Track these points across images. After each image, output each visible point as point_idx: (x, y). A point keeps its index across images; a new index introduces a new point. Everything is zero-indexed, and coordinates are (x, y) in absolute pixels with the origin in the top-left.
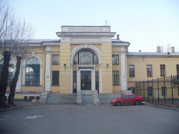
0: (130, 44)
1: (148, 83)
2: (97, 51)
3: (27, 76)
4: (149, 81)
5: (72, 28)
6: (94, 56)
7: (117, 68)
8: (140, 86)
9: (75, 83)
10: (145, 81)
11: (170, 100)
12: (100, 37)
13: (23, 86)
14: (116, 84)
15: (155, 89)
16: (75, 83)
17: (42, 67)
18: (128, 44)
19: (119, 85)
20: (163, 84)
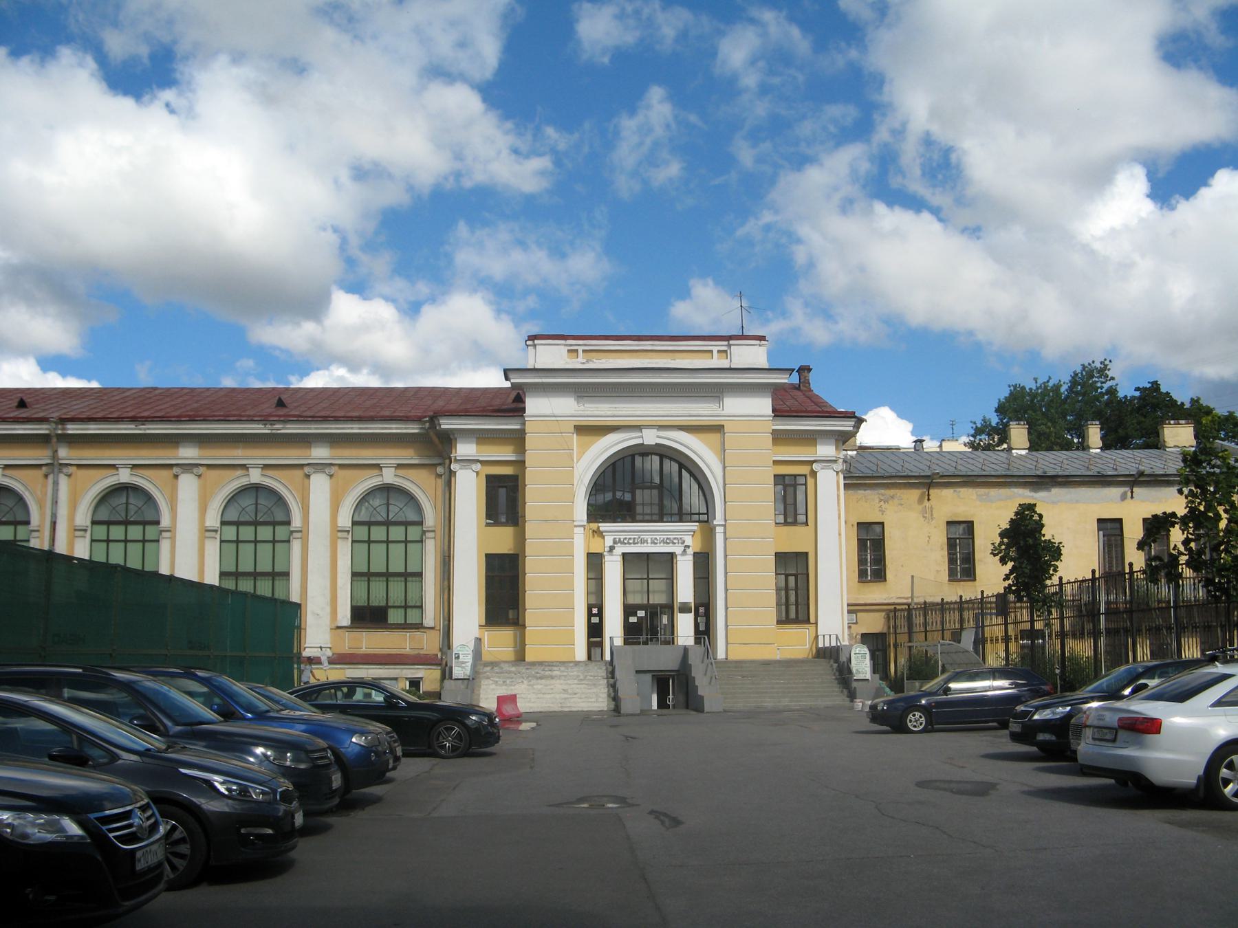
0: (864, 424)
1: (961, 610)
2: (150, 489)
3: (589, 581)
4: (967, 602)
5: (580, 349)
6: (685, 473)
7: (502, 540)
8: (926, 624)
9: (595, 620)
10: (929, 600)
11: (581, 664)
12: (716, 392)
13: (520, 657)
14: (793, 615)
15: (992, 640)
16: (702, 628)
17: (432, 535)
18: (852, 423)
19: (808, 621)
20: (1026, 618)
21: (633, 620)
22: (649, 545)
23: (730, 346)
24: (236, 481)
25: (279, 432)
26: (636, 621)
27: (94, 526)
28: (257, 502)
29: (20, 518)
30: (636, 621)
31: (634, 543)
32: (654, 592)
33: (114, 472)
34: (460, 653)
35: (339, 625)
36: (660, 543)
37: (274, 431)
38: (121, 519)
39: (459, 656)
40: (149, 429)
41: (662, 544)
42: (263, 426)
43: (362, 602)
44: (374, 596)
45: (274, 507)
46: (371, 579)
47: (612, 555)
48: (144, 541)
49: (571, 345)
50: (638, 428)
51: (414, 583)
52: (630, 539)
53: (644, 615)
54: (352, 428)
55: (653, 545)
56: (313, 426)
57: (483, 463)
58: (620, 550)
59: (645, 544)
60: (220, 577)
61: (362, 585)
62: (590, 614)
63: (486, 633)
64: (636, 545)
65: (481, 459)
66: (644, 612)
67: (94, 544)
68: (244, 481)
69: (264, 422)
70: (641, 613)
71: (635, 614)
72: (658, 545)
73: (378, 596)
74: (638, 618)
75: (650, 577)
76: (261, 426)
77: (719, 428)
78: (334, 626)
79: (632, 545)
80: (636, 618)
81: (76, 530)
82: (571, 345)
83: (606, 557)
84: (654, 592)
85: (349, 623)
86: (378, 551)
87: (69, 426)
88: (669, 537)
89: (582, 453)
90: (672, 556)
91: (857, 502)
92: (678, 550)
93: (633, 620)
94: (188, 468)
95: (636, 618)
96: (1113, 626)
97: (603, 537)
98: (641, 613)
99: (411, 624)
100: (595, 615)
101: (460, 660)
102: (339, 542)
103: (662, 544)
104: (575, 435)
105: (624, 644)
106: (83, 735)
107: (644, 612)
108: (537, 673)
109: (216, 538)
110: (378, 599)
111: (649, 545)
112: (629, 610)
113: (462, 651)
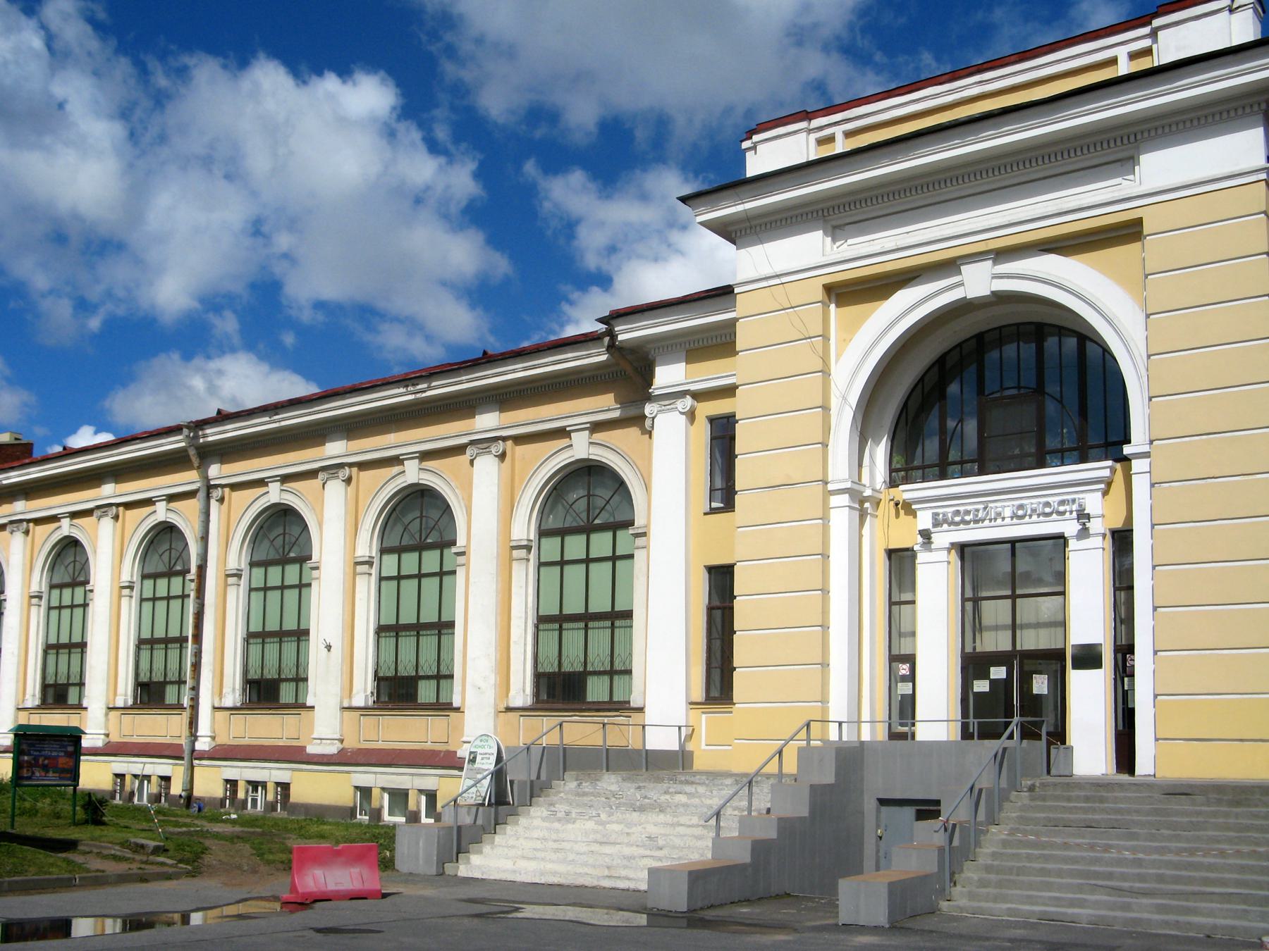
9: (904, 688)
21: (981, 686)
22: (1008, 521)
23: (1154, 34)
24: (550, 459)
25: (424, 395)
26: (987, 689)
27: (543, 540)
28: (589, 492)
29: (620, 517)
30: (987, 689)
31: (976, 522)
32: (1004, 627)
33: (563, 442)
34: (479, 751)
35: (512, 705)
36: (1030, 516)
37: (419, 396)
38: (582, 524)
39: (475, 758)
40: (284, 419)
41: (1035, 518)
42: (404, 390)
43: (550, 666)
44: (285, 664)
45: (287, 528)
46: (283, 639)
47: (931, 550)
48: (614, 559)
49: (821, 128)
50: (949, 266)
51: (289, 643)
52: (968, 512)
53: (1004, 676)
54: (514, 371)
55: (1015, 521)
56: (464, 378)
57: (698, 396)
58: (943, 538)
59: (999, 521)
60: (537, 627)
61: (388, 643)
62: (893, 679)
63: (704, 716)
64: (980, 525)
65: (693, 387)
66: (1004, 668)
67: (543, 569)
68: (401, 482)
69: (404, 383)
70: (998, 673)
71: (985, 675)
72: (1027, 519)
73: (289, 664)
74: (994, 683)
75: (1018, 592)
76: (402, 390)
77: (1130, 231)
78: (502, 708)
79: (962, 526)
80: (987, 682)
81: (228, 576)
82: (821, 128)
83: (919, 555)
84: (1004, 627)
85: (704, 699)
86: (575, 574)
87: (208, 431)
88: (969, 508)
89: (845, 342)
90: (1061, 539)
91: (12, 533)
92: (1069, 527)
93: (981, 686)
94: (483, 444)
95: (987, 682)
96: (1002, 713)
97: (915, 517)
98: (998, 673)
99: (594, 702)
100: (904, 679)
101: (476, 766)
102: (515, 564)
103: (1035, 518)
104: (833, 306)
105: (962, 738)
106: (1040, 897)
107: (1004, 668)
108: (645, 797)
109: (370, 574)
110: (572, 663)
111: (1008, 521)
112: (973, 665)
113: (483, 747)
